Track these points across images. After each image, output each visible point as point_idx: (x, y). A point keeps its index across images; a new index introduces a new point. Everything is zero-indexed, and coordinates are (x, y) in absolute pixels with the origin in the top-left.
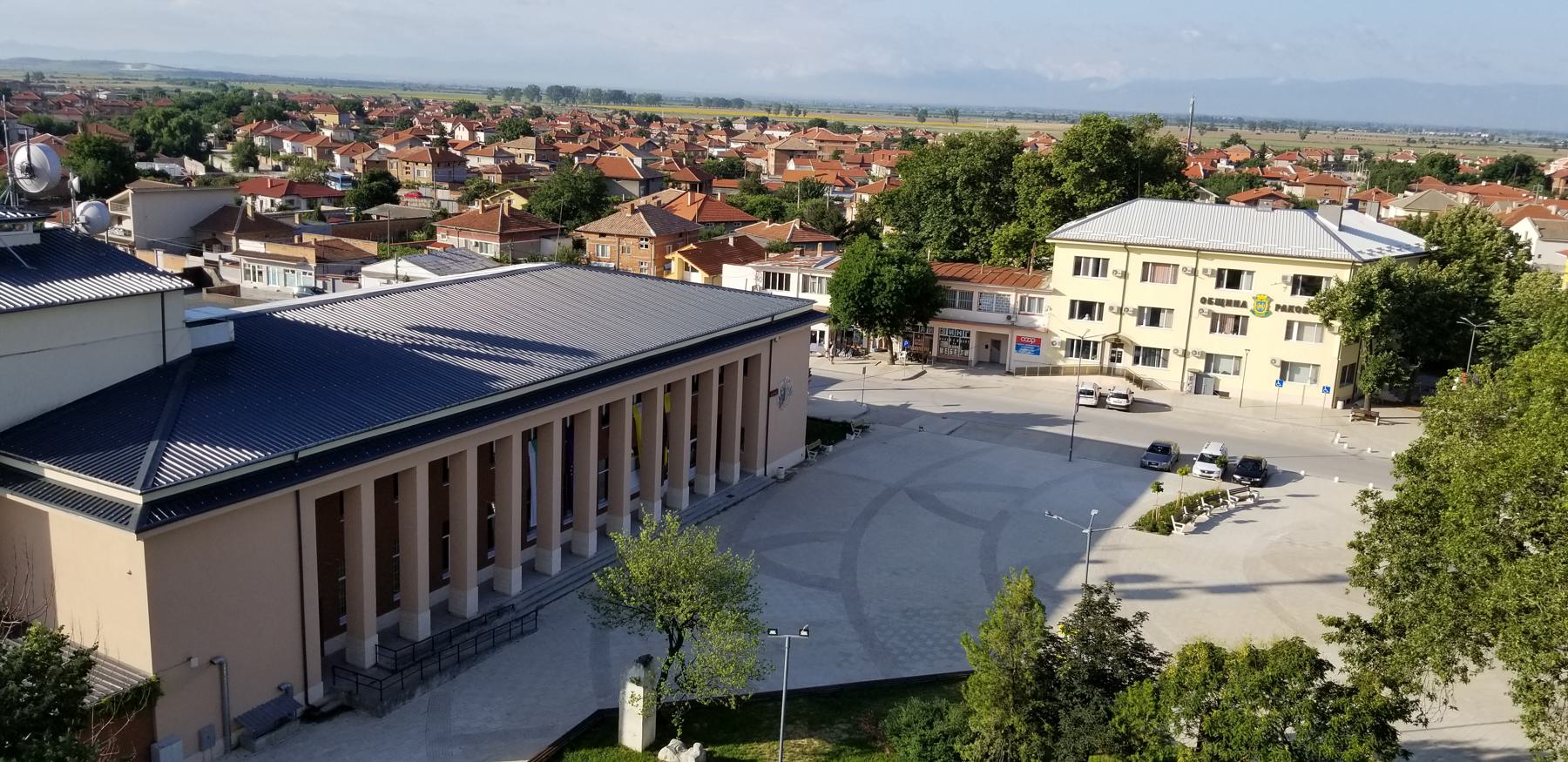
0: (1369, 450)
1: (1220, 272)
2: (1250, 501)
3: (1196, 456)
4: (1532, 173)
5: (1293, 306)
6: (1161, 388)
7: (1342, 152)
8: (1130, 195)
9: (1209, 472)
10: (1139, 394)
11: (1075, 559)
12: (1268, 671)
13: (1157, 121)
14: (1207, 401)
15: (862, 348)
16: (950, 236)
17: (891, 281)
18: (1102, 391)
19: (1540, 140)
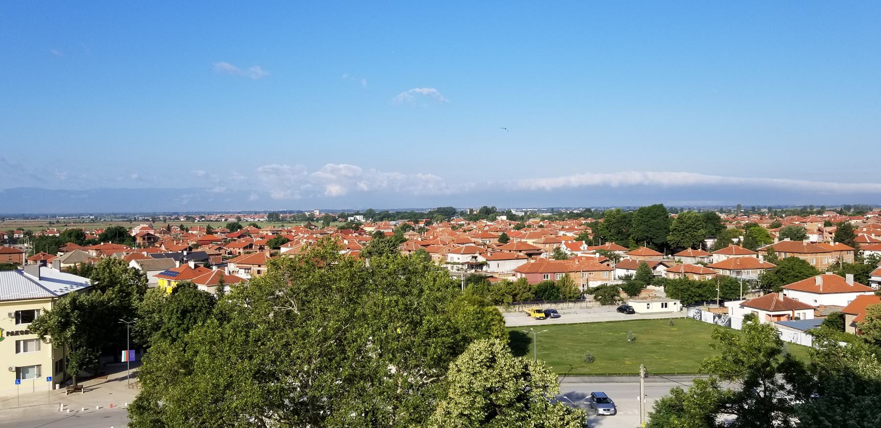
0: (83, 409)
4: (125, 235)
5: (18, 331)
7: (13, 232)
19: (121, 218)
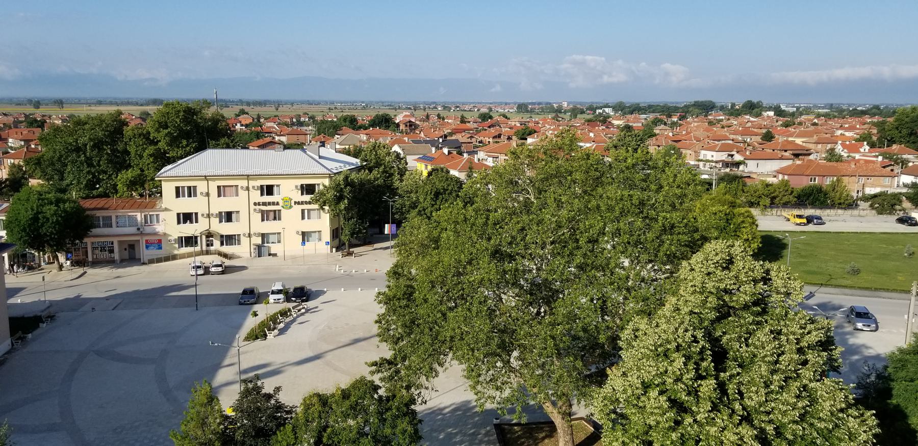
0: (354, 271)
1: (262, 186)
2: (303, 311)
3: (269, 292)
6: (239, 257)
7: (300, 116)
8: (201, 147)
9: (278, 300)
10: (228, 263)
11: (217, 367)
12: (353, 399)
13: (208, 104)
14: (266, 260)
15: (35, 264)
16: (87, 182)
17: (52, 215)
18: (205, 265)
19: (388, 105)
